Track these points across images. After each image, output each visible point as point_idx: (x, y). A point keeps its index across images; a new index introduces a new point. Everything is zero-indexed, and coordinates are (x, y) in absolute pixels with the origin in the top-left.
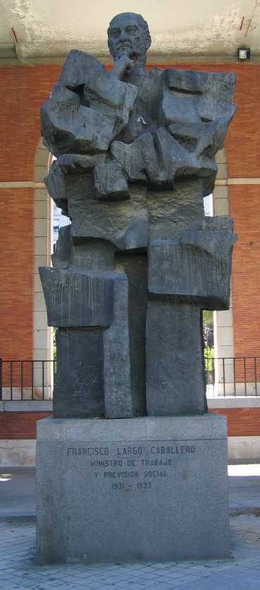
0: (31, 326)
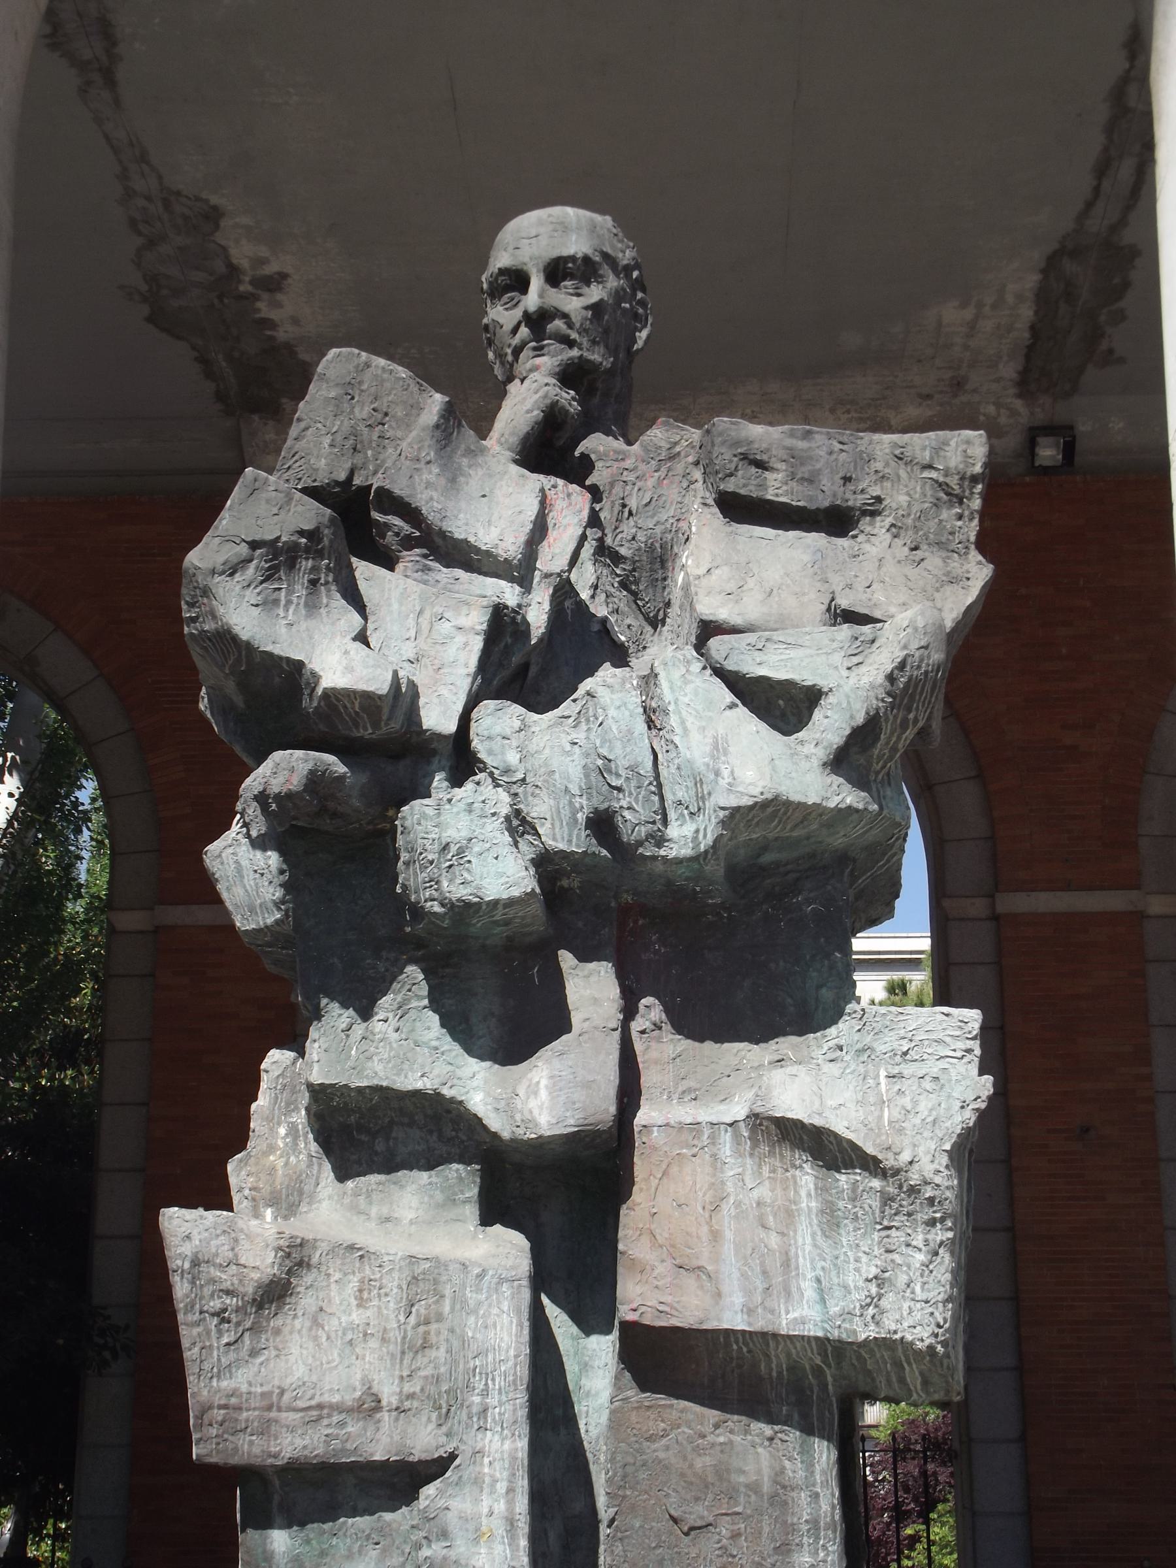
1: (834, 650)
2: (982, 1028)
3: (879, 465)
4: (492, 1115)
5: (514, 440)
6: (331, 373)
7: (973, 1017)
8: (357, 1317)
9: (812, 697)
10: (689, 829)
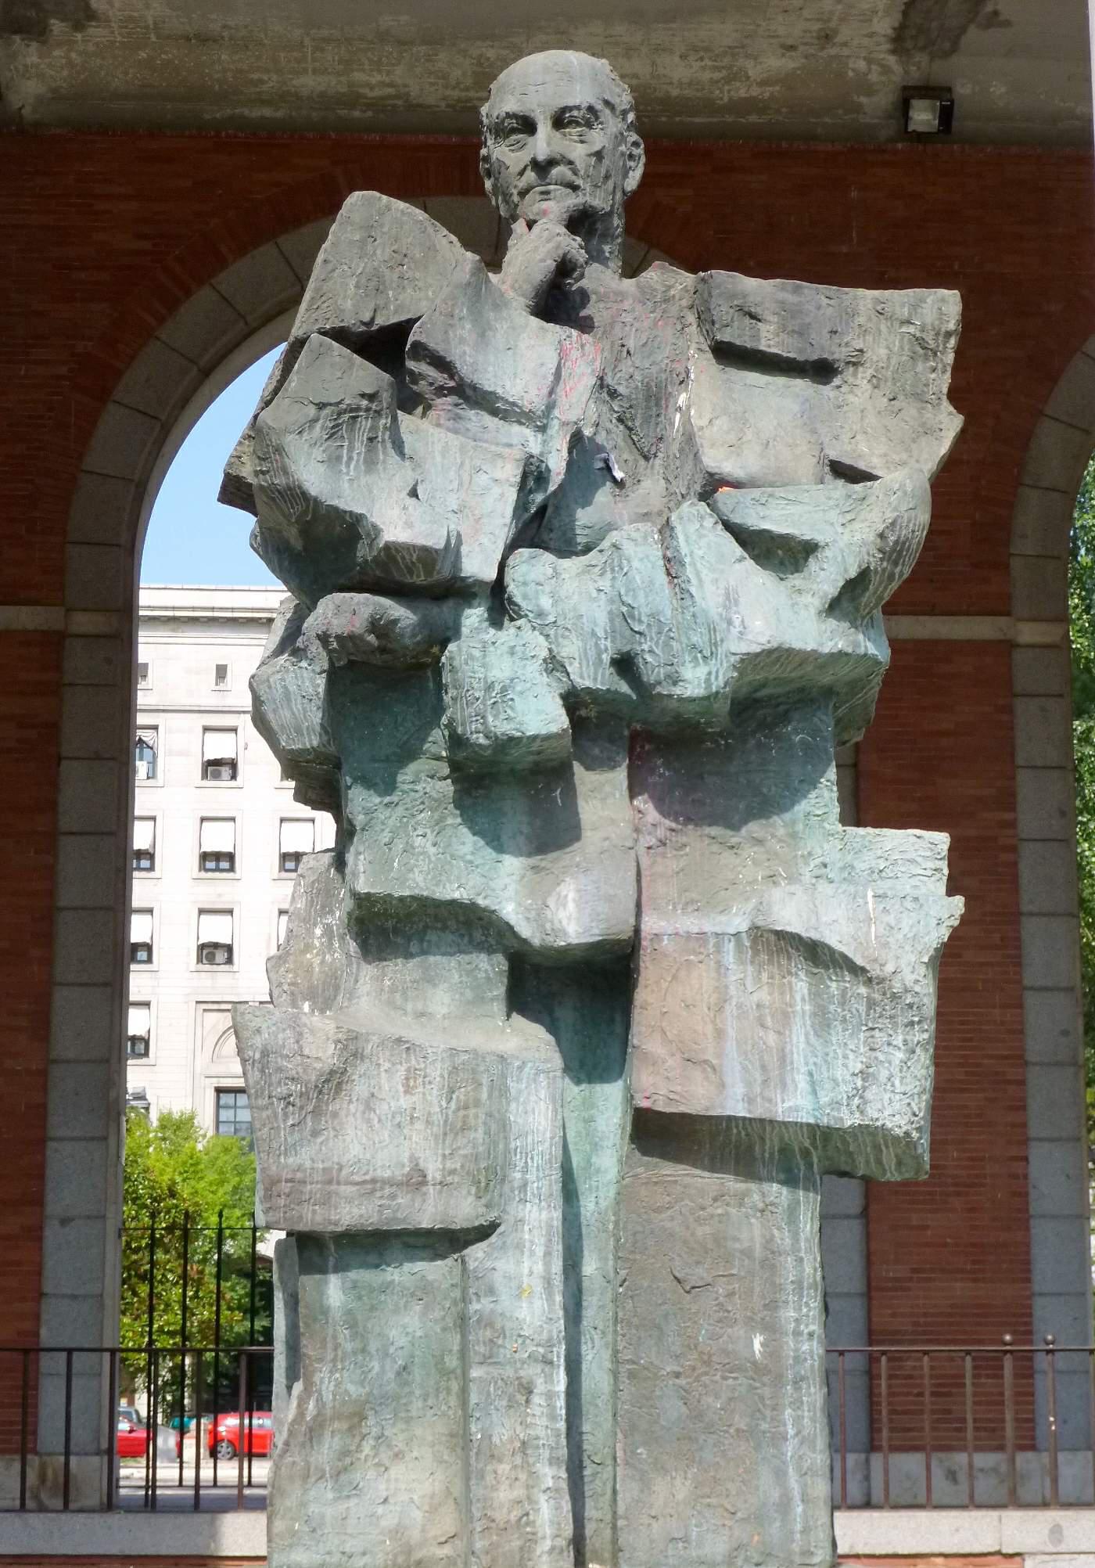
0: (38, 1201)
1: (831, 508)
2: (950, 850)
3: (861, 320)
4: (524, 923)
5: (529, 289)
6: (356, 217)
7: (942, 840)
8: (404, 1102)
9: (809, 549)
10: (702, 671)
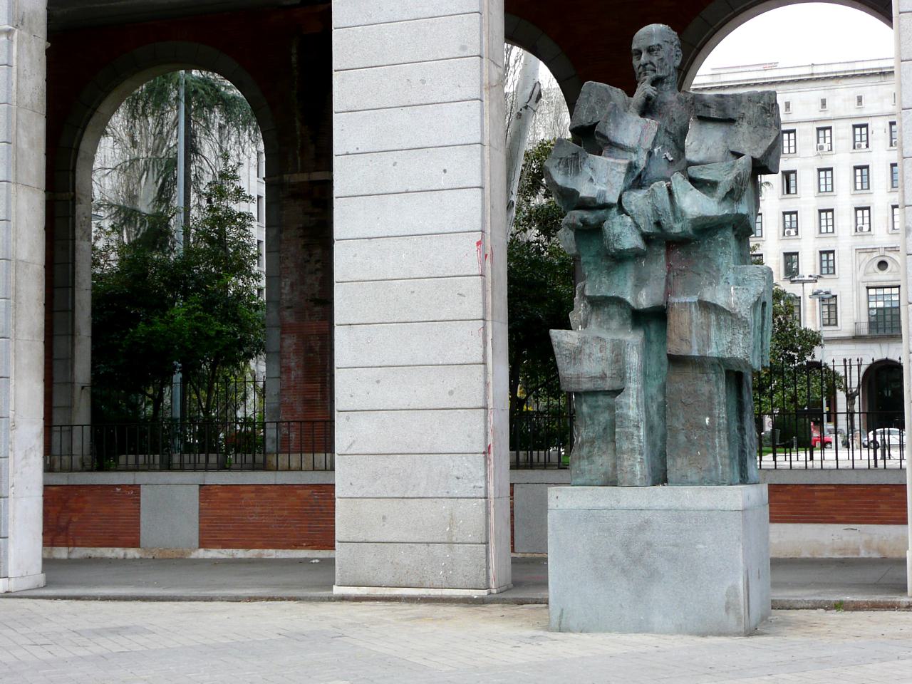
3: (744, 104)
8: (600, 355)
